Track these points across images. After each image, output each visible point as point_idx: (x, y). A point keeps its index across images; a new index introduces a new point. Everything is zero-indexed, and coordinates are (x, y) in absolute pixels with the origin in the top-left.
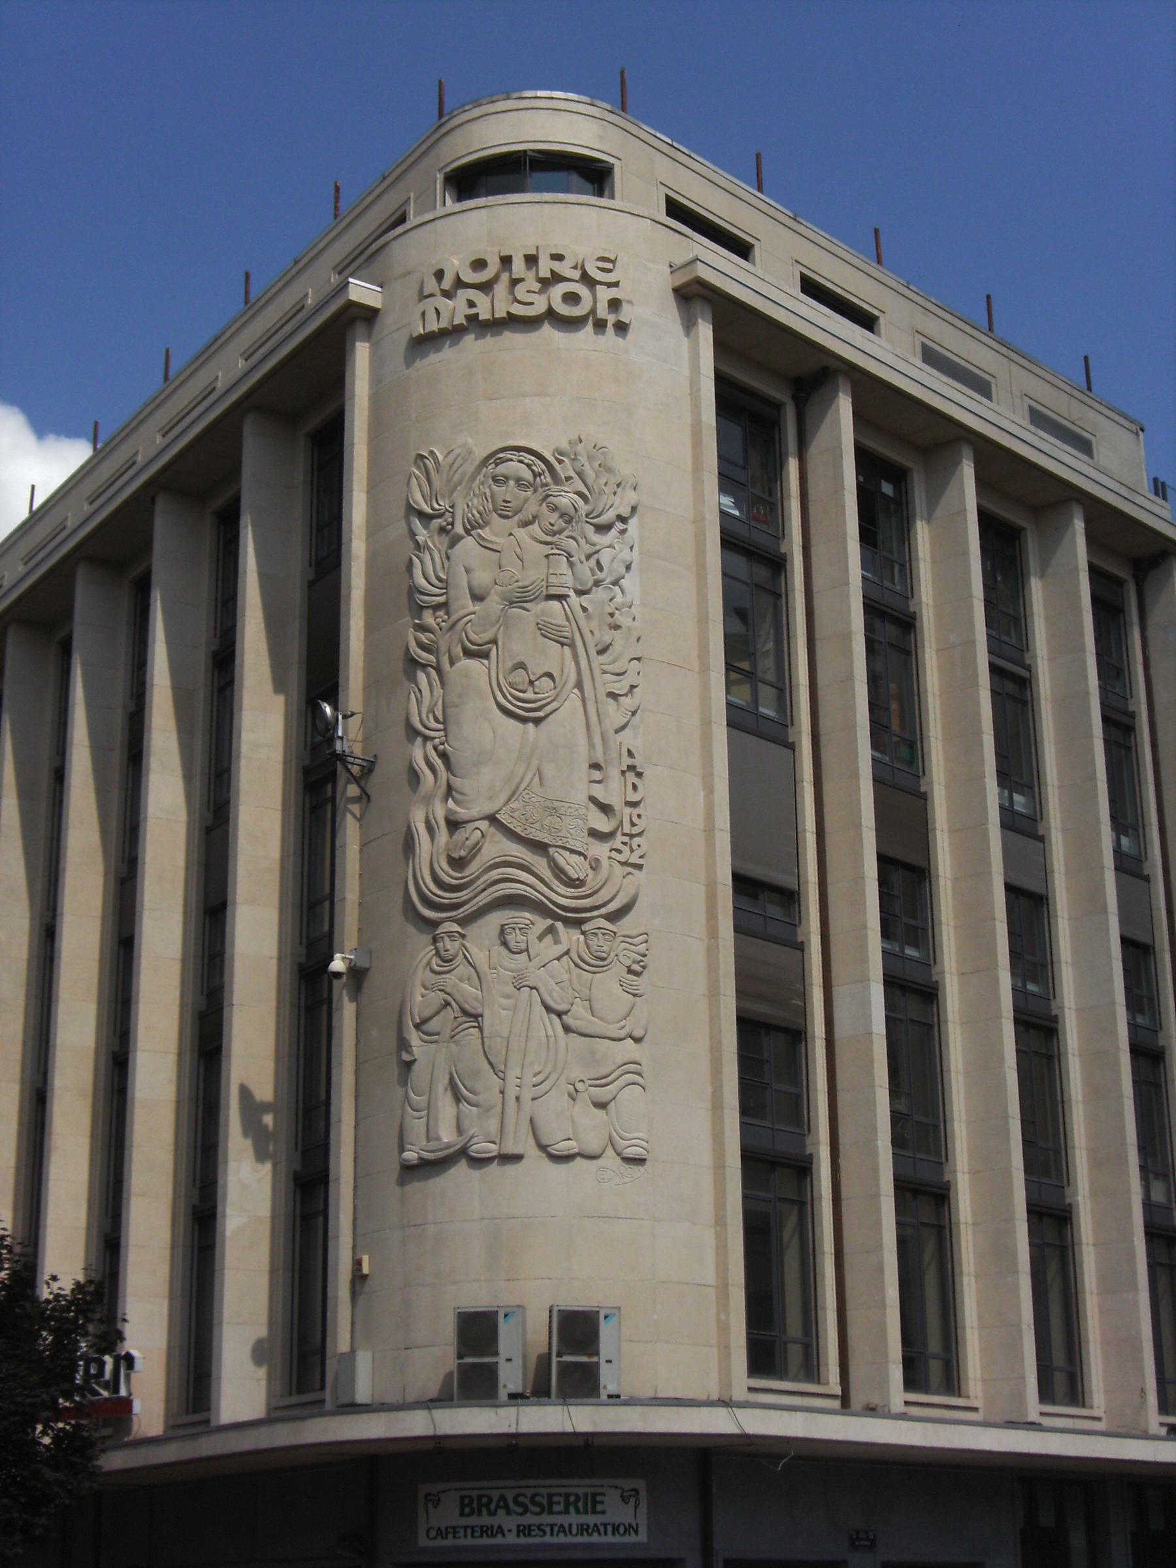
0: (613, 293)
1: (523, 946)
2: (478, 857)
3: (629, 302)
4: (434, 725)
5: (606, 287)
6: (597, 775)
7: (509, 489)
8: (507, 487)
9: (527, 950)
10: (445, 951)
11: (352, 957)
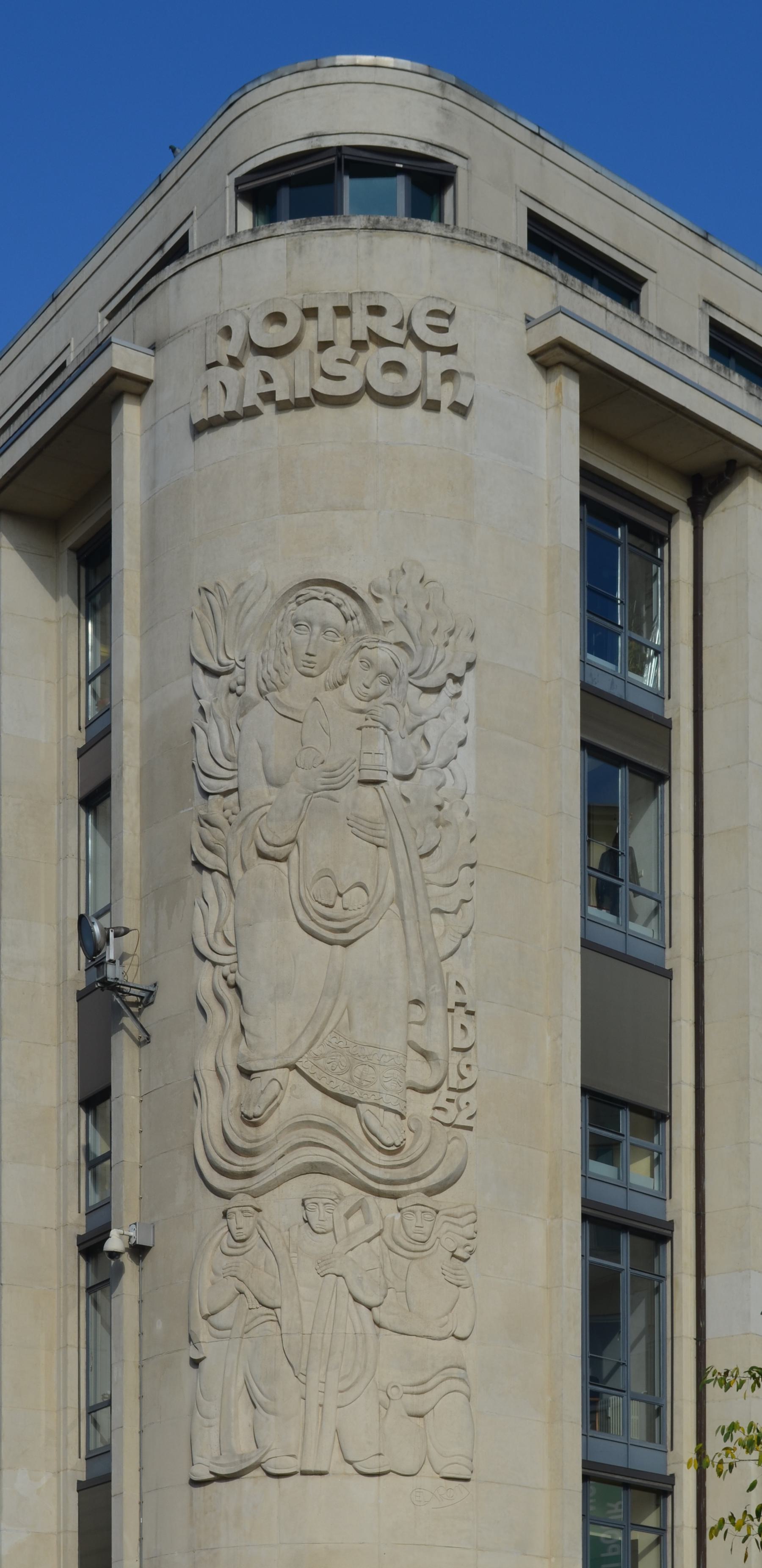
0: (449, 363)
1: (328, 1225)
2: (275, 1114)
3: (470, 375)
4: (221, 947)
5: (439, 354)
6: (418, 1013)
7: (314, 638)
8: (311, 635)
9: (333, 1230)
10: (237, 1229)
11: (132, 1234)
